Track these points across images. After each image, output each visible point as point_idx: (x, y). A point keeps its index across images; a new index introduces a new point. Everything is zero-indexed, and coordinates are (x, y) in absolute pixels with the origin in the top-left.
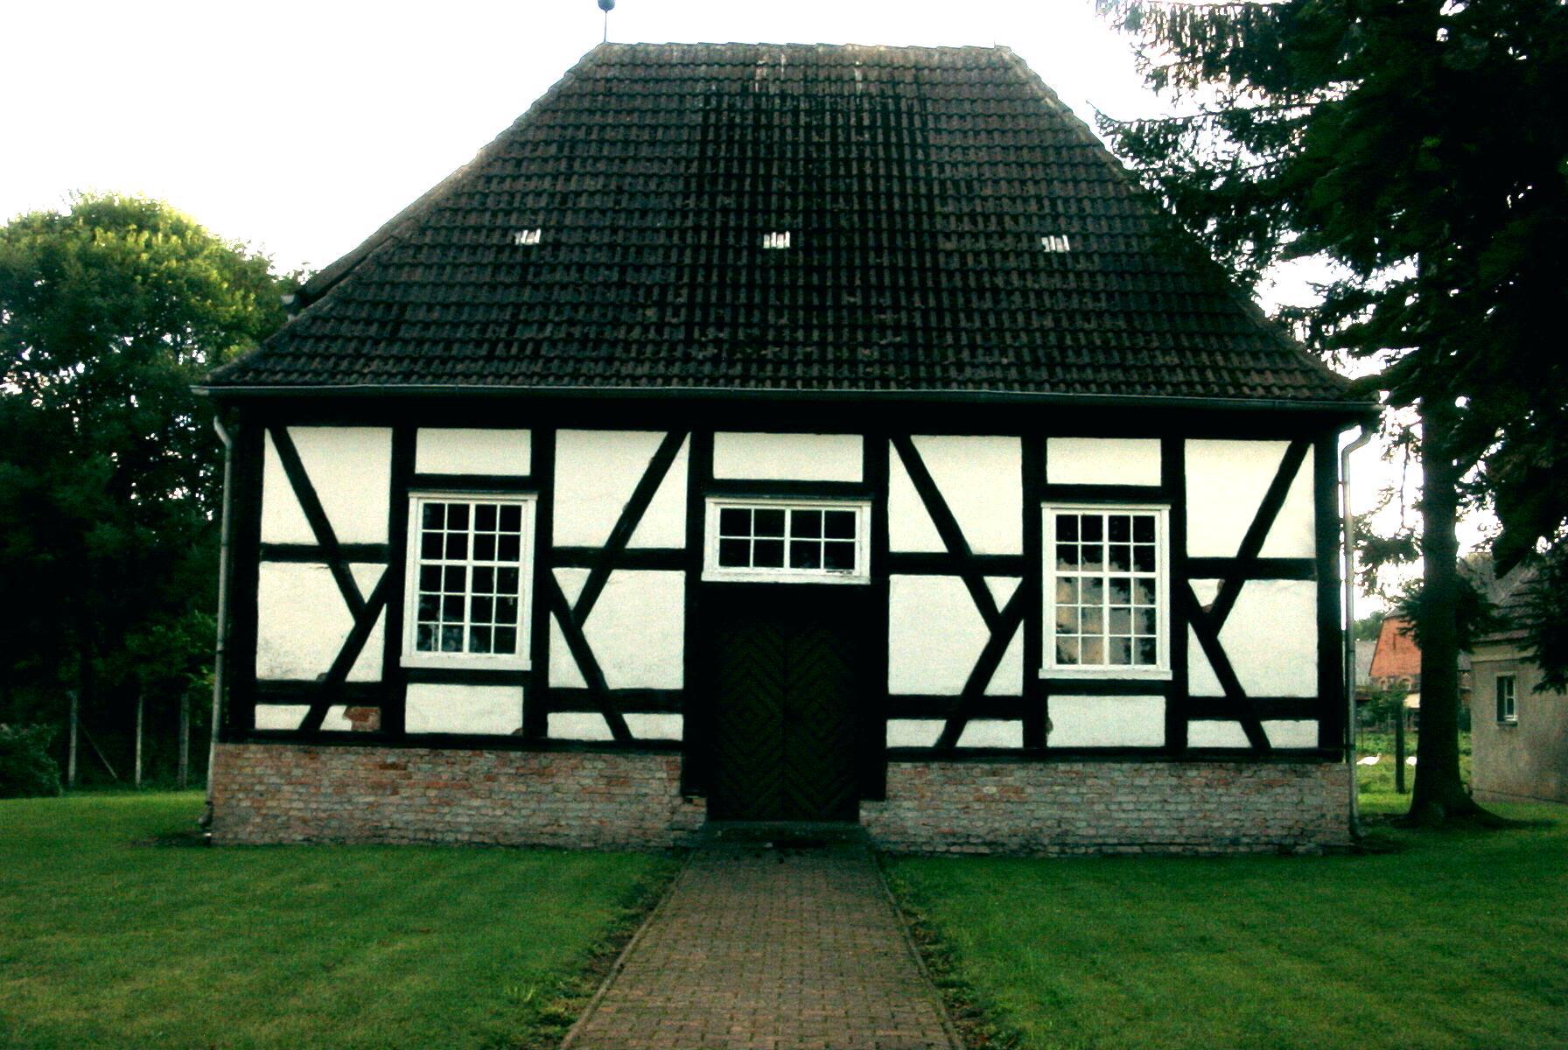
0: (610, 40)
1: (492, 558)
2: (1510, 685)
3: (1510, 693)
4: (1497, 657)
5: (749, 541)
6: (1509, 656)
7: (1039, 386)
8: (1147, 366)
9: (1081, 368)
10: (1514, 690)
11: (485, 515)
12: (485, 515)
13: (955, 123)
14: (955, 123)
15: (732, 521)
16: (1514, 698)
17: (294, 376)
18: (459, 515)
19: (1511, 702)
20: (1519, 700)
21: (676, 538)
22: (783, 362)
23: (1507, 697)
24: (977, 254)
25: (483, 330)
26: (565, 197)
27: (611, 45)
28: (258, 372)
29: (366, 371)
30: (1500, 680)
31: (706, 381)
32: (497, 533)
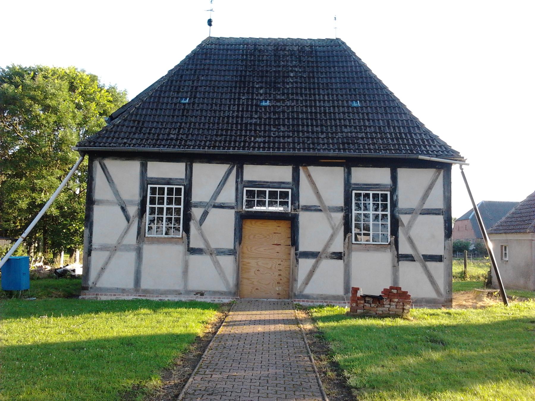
0: (211, 36)
1: (155, 204)
2: (505, 247)
3: (505, 250)
4: (501, 238)
5: (175, 195)
6: (504, 239)
7: (299, 150)
8: (366, 144)
9: (324, 144)
10: (507, 249)
11: (170, 191)
12: (375, 196)
13: (323, 64)
14: (323, 64)
15: (250, 194)
16: (507, 252)
17: (107, 144)
18: (162, 190)
19: (506, 253)
20: (509, 253)
21: (440, 205)
22: (266, 142)
23: (504, 252)
24: (329, 107)
25: (150, 130)
26: (197, 87)
27: (211, 37)
28: (95, 143)
29: (145, 143)
30: (502, 246)
31: (192, 147)
32: (174, 196)
